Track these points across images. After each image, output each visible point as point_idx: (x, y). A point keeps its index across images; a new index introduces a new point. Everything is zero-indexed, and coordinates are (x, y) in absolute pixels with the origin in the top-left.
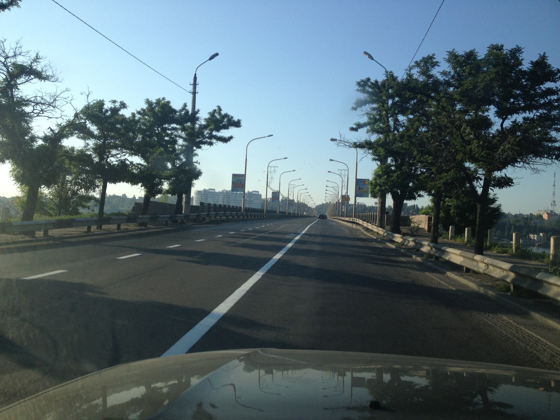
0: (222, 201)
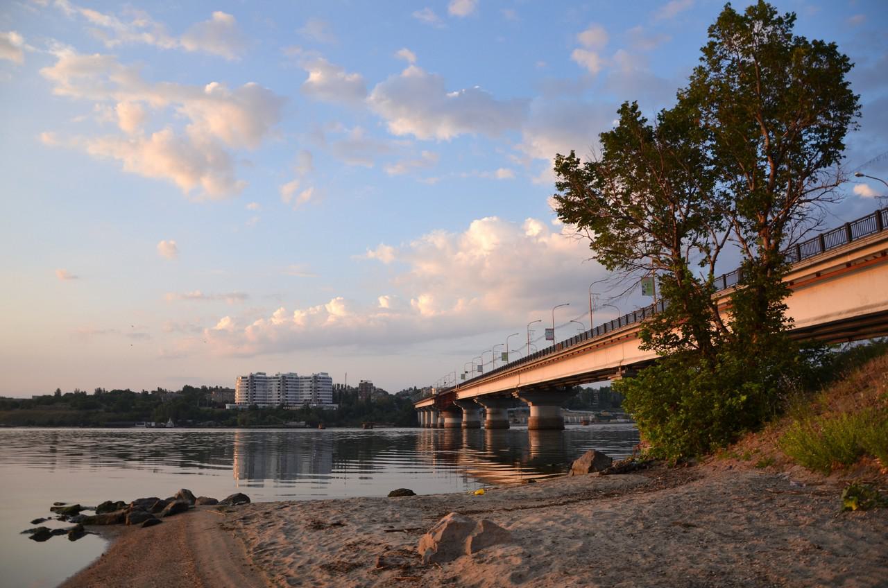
0: (277, 389)
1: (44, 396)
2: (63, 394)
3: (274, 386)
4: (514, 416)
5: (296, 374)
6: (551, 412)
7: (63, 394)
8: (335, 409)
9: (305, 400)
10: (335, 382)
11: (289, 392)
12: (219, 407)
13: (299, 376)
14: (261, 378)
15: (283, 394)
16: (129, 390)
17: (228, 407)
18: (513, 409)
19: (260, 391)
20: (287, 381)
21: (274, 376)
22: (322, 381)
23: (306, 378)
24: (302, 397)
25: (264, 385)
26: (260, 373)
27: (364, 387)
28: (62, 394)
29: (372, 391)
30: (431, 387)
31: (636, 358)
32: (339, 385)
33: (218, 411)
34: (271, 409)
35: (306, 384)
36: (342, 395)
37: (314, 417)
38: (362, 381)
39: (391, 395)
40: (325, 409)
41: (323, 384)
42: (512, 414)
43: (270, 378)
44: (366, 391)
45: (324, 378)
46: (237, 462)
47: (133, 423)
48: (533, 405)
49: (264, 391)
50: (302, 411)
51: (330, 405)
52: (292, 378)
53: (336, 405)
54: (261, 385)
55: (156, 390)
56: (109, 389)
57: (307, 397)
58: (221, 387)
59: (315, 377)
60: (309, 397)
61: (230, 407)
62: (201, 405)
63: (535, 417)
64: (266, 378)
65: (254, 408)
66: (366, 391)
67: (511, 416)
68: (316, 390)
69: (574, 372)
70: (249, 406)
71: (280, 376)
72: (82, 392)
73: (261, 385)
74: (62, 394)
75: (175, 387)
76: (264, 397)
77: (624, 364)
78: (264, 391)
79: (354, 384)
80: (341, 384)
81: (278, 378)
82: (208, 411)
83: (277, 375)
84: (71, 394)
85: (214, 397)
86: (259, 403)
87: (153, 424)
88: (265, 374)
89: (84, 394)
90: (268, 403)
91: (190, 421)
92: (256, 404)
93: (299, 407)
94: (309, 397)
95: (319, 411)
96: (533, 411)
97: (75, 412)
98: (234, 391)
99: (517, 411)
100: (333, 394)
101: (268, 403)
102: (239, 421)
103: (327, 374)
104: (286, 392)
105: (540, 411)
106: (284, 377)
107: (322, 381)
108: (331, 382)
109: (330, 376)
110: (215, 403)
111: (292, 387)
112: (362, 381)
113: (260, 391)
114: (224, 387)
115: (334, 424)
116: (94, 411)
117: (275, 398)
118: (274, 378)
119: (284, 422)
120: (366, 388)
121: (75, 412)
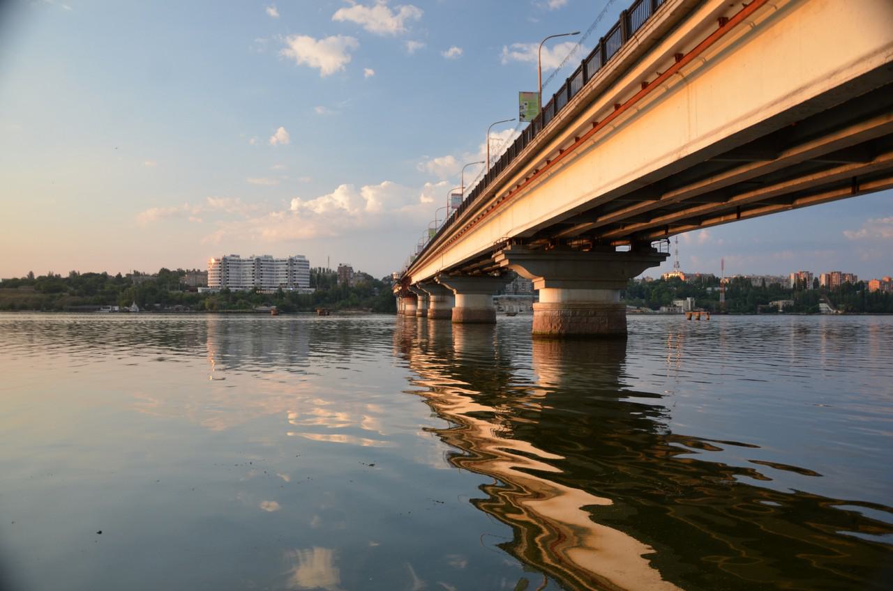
1: (90, 275)
2: (36, 277)
3: (249, 269)
4: (497, 304)
5: (271, 257)
6: (481, 302)
7: (36, 277)
8: (310, 293)
9: (281, 284)
10: (313, 266)
11: (264, 275)
12: (192, 291)
13: (274, 258)
14: (234, 260)
15: (258, 278)
16: (106, 273)
17: (200, 290)
18: (497, 296)
19: (233, 274)
20: (262, 264)
21: (249, 259)
22: (298, 264)
23: (282, 261)
24: (277, 281)
25: (238, 267)
26: (233, 256)
27: (343, 271)
28: (36, 277)
29: (352, 275)
30: (392, 275)
31: (518, 228)
32: (320, 269)
33: (188, 294)
34: (243, 293)
35: (283, 267)
36: (320, 279)
37: (289, 303)
38: (341, 265)
39: (376, 280)
40: (299, 293)
41: (300, 268)
42: (496, 302)
43: (244, 261)
44: (345, 275)
45: (300, 261)
46: (211, 346)
47: (98, 307)
48: (547, 286)
49: (238, 274)
50: (275, 295)
51: (306, 289)
52: (267, 261)
53: (313, 290)
54: (234, 267)
55: (133, 273)
56: (82, 271)
57: (283, 280)
58: (199, 270)
59: (291, 260)
60: (284, 281)
61: (202, 290)
62: (173, 288)
63: (459, 308)
64: (240, 261)
65: (226, 292)
66: (345, 275)
67: (496, 304)
68: (291, 273)
69: (477, 250)
70: (221, 290)
71: (254, 259)
72: (56, 275)
73: (234, 267)
74: (36, 277)
75: (152, 269)
76: (237, 280)
77: (511, 236)
78: (238, 274)
79: (335, 268)
80: (322, 267)
81: (252, 261)
82: (177, 294)
83: (251, 257)
84: (45, 277)
85: (187, 281)
86: (232, 287)
87: (117, 308)
88: (238, 256)
89: (58, 277)
90: (242, 287)
91: (158, 305)
92: (228, 287)
93: (273, 291)
94: (284, 281)
95: (294, 296)
96: (547, 297)
97: (38, 295)
98: (206, 274)
99: (502, 298)
100: (310, 281)
101: (242, 287)
102: (207, 305)
103: (303, 257)
104: (260, 276)
105: (466, 301)
106: (258, 259)
107: (298, 264)
108: (308, 265)
109: (307, 259)
110: (188, 287)
111: (267, 271)
112: (341, 265)
113: (233, 274)
114: (146, 273)
115: (308, 309)
116: (57, 294)
117: (249, 283)
118: (248, 261)
119: (254, 307)
120: (345, 272)
121: (38, 295)
